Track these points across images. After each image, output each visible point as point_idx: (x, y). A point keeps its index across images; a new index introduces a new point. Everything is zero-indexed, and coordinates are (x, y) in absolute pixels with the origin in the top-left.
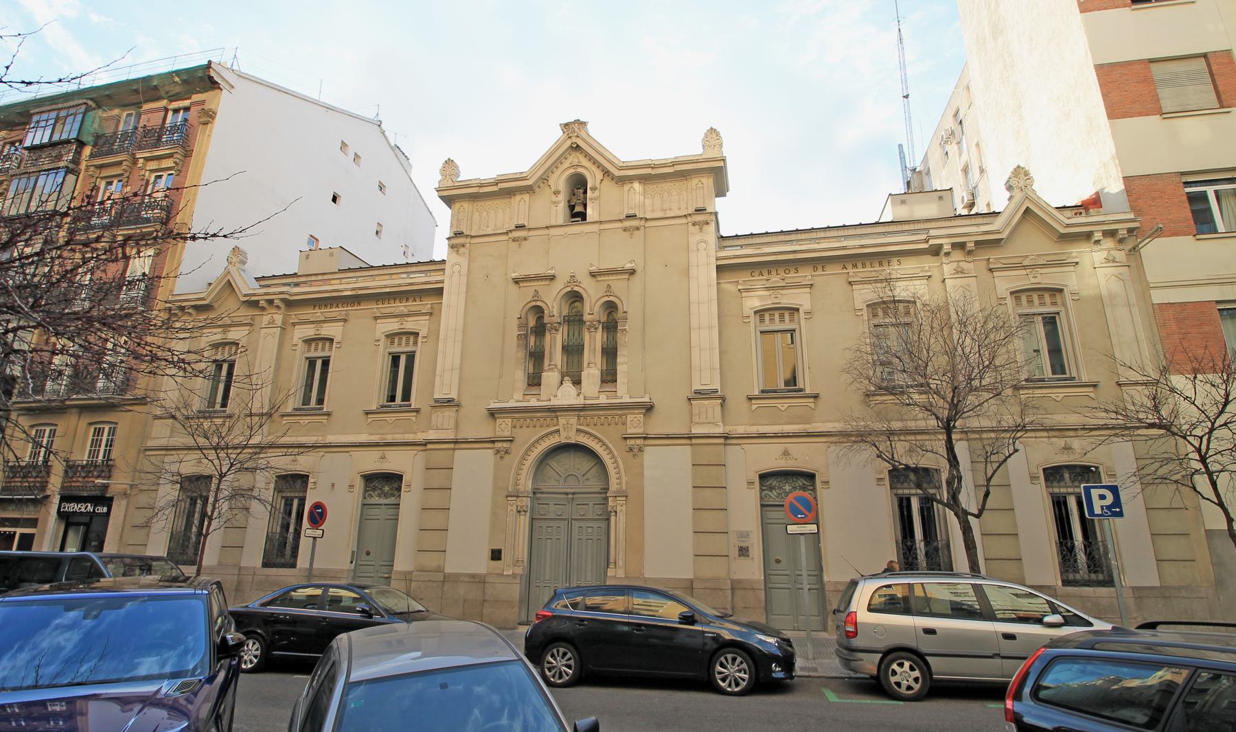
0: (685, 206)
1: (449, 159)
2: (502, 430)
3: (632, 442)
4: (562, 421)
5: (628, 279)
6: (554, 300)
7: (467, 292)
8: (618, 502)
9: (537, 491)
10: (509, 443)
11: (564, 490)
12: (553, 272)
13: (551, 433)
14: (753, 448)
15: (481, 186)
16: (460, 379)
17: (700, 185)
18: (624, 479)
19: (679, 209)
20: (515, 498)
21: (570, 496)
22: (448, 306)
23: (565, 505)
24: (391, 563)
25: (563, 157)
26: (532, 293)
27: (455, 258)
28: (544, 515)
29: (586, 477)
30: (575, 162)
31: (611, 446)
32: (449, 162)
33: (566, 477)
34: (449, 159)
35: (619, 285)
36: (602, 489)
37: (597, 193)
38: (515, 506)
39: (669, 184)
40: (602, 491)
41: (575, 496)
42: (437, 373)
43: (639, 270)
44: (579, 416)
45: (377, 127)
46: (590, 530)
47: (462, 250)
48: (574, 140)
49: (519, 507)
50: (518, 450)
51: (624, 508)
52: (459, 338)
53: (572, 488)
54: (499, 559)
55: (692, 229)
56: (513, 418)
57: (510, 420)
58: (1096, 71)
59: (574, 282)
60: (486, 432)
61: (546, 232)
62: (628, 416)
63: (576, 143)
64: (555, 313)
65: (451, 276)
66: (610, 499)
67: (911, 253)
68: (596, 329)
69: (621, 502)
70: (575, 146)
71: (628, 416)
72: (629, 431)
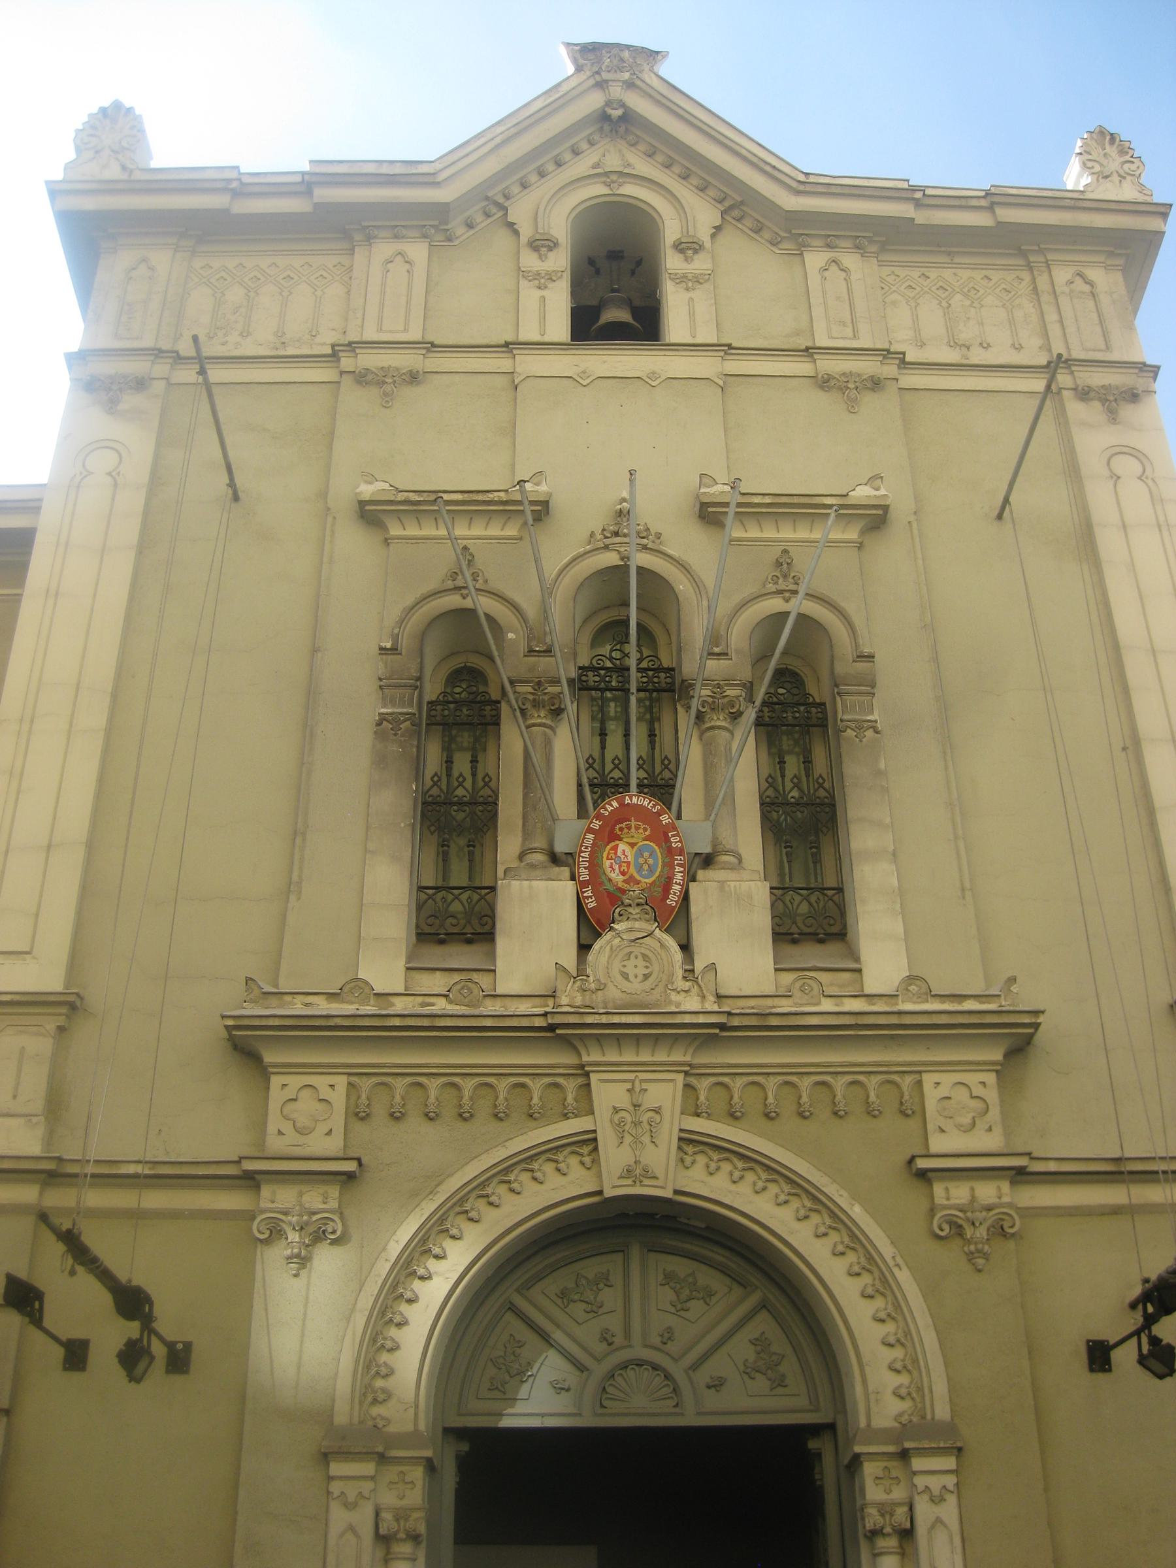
2: (300, 1131)
3: (959, 1193)
5: (860, 546)
10: (334, 1191)
12: (543, 488)
13: (552, 1150)
16: (86, 892)
17: (1080, 285)
19: (1018, 348)
20: (368, 1468)
26: (446, 557)
29: (703, 1376)
30: (613, 162)
37: (700, 264)
39: (965, 274)
43: (901, 508)
48: (616, 91)
49: (387, 1516)
51: (949, 1511)
52: (94, 716)
56: (355, 1073)
57: (341, 1081)
61: (502, 363)
62: (925, 1077)
63: (622, 105)
66: (870, 1469)
68: (736, 716)
69: (935, 1483)
70: (616, 113)
71: (928, 1080)
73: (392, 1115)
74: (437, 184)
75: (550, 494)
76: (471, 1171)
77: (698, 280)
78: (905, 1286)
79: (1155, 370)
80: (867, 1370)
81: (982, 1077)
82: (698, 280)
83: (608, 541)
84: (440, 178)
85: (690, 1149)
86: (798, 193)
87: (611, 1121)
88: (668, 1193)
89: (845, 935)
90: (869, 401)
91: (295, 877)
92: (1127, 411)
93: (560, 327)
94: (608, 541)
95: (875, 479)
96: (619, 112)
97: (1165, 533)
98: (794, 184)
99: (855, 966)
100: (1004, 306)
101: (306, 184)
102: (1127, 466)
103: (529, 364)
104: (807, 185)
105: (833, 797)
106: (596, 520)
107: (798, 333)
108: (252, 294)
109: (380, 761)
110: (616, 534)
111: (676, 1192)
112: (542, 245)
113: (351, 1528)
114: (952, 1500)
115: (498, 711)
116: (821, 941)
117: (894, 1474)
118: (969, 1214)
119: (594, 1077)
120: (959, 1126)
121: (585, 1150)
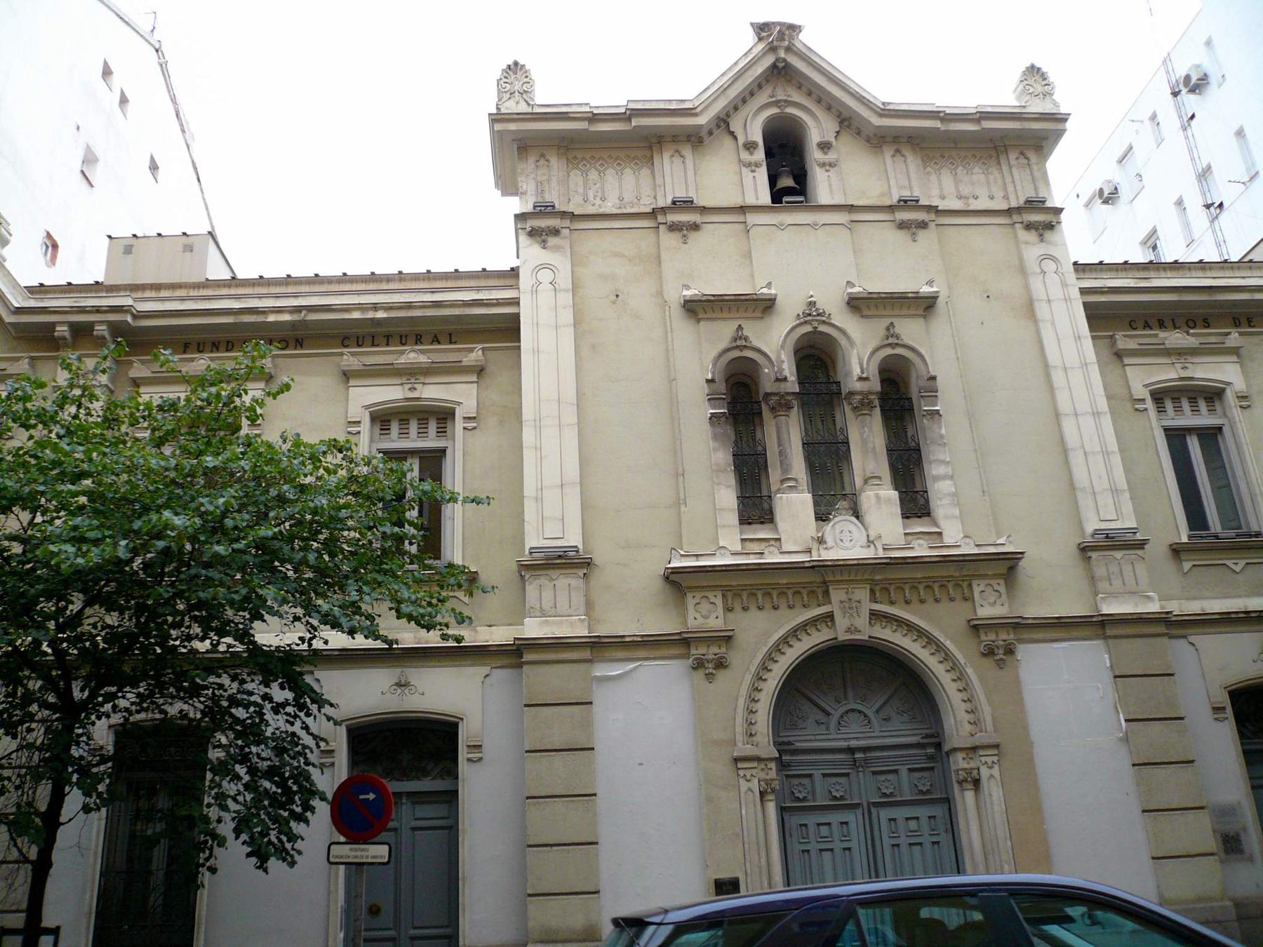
0: (1002, 194)
1: (710, 677)
4: (837, 595)
6: (782, 347)
7: (576, 324)
8: (983, 759)
9: (786, 747)
11: (844, 744)
13: (814, 622)
14: (1213, 644)
15: (594, 118)
16: (585, 507)
18: (987, 712)
19: (992, 198)
21: (858, 755)
22: (537, 352)
23: (847, 775)
24: (448, 931)
25: (759, 85)
27: (534, 253)
28: (805, 799)
30: (781, 96)
31: (948, 643)
32: (515, 68)
33: (853, 710)
34: (710, 677)
35: (910, 330)
36: (927, 736)
37: (831, 156)
38: (756, 781)
40: (925, 741)
41: (869, 755)
42: (526, 493)
44: (873, 583)
45: (154, 51)
47: (552, 241)
48: (782, 54)
50: (745, 660)
51: (996, 771)
52: (571, 417)
55: (1023, 235)
59: (818, 315)
60: (660, 623)
62: (973, 582)
63: (784, 60)
64: (787, 373)
65: (535, 291)
67: (485, 331)
69: (989, 760)
73: (743, 608)
74: (696, 115)
75: (776, 295)
76: (781, 632)
77: (832, 165)
78: (971, 676)
79: (1061, 210)
80: (956, 712)
81: (999, 581)
82: (832, 165)
83: (806, 319)
84: (698, 110)
85: (873, 617)
86: (881, 116)
87: (840, 607)
88: (867, 638)
89: (929, 513)
90: (922, 234)
91: (682, 496)
92: (1048, 235)
93: (765, 198)
94: (806, 319)
95: (930, 283)
96: (783, 64)
97: (1069, 303)
98: (878, 110)
99: (937, 530)
100: (983, 173)
101: (630, 114)
102: (1049, 266)
103: (752, 218)
104: (886, 112)
105: (919, 445)
106: (800, 308)
107: (882, 195)
108: (602, 175)
109: (715, 437)
110: (810, 315)
111: (870, 637)
112: (750, 146)
113: (750, 789)
114: (996, 767)
115: (760, 406)
116: (920, 517)
117: (970, 756)
118: (996, 643)
119: (831, 587)
120: (989, 603)
121: (828, 620)
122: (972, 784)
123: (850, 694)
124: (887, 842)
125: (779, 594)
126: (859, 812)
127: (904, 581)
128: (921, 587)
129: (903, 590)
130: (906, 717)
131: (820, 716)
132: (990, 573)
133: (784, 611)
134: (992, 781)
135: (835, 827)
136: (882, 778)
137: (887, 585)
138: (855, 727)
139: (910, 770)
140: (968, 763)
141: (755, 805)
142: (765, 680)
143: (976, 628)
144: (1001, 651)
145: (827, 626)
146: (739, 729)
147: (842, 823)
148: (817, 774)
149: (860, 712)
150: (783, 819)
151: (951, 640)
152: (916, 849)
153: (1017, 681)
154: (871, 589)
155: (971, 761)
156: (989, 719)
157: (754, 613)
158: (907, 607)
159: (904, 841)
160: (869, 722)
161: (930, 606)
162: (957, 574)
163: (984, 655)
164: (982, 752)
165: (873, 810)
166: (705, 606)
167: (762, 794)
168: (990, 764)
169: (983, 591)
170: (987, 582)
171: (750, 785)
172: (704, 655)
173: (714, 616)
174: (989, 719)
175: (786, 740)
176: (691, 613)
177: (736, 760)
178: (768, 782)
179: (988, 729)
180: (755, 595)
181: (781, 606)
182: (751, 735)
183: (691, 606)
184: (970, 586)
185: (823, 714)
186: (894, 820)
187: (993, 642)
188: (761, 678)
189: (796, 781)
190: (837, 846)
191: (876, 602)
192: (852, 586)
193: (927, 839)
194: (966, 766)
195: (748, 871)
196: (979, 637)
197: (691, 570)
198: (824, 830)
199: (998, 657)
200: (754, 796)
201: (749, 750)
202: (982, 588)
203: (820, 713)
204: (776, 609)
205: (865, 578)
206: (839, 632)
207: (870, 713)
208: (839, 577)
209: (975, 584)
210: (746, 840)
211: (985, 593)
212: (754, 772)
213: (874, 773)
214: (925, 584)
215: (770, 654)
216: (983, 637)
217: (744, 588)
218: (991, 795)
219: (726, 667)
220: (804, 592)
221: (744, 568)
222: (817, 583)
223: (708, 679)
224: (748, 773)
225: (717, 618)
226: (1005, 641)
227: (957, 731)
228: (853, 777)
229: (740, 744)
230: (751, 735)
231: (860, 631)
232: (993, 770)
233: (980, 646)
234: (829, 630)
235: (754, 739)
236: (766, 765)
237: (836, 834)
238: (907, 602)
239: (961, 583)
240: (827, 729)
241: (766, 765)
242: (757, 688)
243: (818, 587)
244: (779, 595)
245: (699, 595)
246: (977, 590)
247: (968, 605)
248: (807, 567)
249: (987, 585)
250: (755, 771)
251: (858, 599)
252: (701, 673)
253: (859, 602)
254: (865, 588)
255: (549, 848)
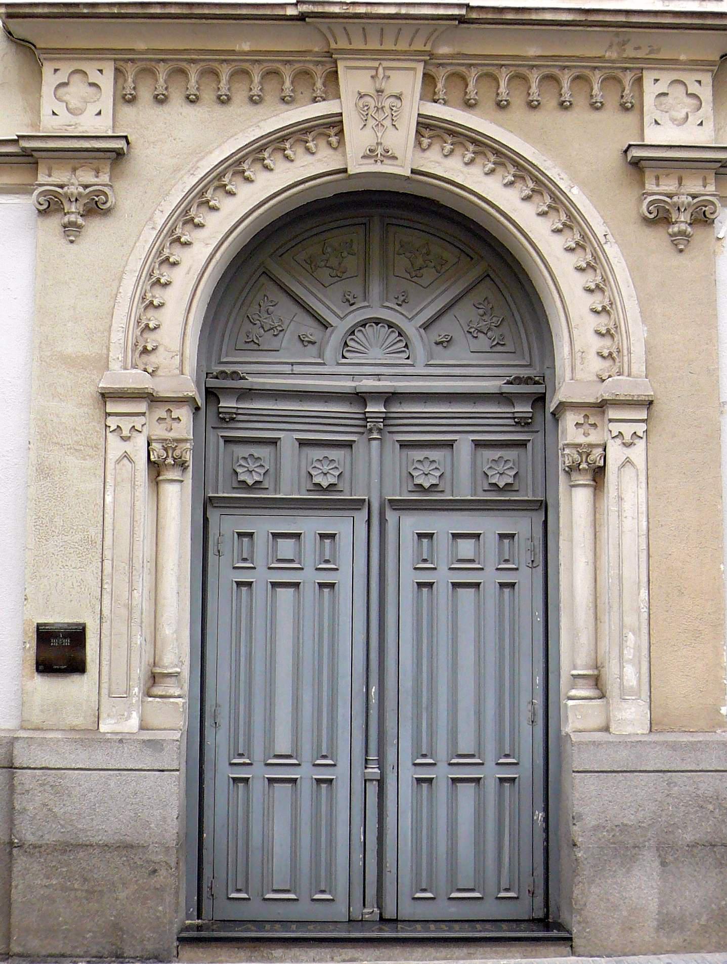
1: (71, 230)
8: (615, 428)
11: (346, 385)
21: (373, 408)
23: (349, 445)
31: (575, 194)
33: (377, 322)
34: (71, 230)
36: (518, 380)
38: (140, 441)
41: (396, 408)
44: (430, 59)
46: (466, 548)
53: (378, 376)
54: (77, 666)
58: (32, 645)
69: (627, 430)
72: (653, 136)
85: (427, 133)
88: (408, 173)
111: (413, 171)
113: (126, 456)
117: (591, 421)
119: (341, 66)
120: (673, 120)
121: (332, 131)
122: (589, 477)
123: (375, 289)
124: (409, 578)
125: (232, 75)
126: (362, 515)
127: (500, 62)
128: (534, 78)
129: (496, 80)
130: (483, 342)
131: (311, 330)
132: (683, 57)
133: (239, 108)
134: (629, 471)
135: (309, 542)
136: (419, 454)
137: (463, 69)
138: (376, 354)
139: (478, 444)
140: (586, 434)
141: (133, 487)
142: (187, 244)
143: (637, 165)
144: (684, 217)
145: (330, 144)
146: (117, 337)
147: (323, 536)
148: (288, 440)
149: (391, 325)
150: (206, 520)
151: (583, 185)
152: (467, 594)
153: (710, 281)
154: (425, 75)
155: (592, 431)
156: (638, 351)
157: (177, 107)
158: (500, 115)
159: (443, 578)
160: (406, 346)
161: (548, 117)
162: (612, 54)
163: (650, 222)
164: (612, 414)
165: (391, 516)
166: (77, 91)
167: (155, 468)
168: (628, 438)
169: (665, 94)
170: (675, 76)
171: (127, 447)
172: (62, 187)
173: (92, 109)
174: (638, 351)
175: (229, 369)
176: (48, 103)
177: (106, 396)
178: (169, 445)
179: (635, 369)
180: (183, 72)
181: (608, 105)
182: (145, 351)
183: (47, 89)
184: (639, 81)
185: (315, 324)
186: (430, 536)
187: (670, 196)
188: (178, 239)
189: (242, 451)
190: (309, 577)
191: (435, 101)
192: (386, 64)
193: (490, 578)
194: (581, 440)
195: (106, 612)
196: (643, 185)
197: (46, 10)
198: (286, 548)
199: (675, 229)
200: (134, 470)
201: (135, 379)
202: (662, 87)
203: (310, 321)
204: (223, 102)
205: (413, 48)
206: (349, 161)
207: (410, 329)
208: (358, 44)
209: (648, 78)
210: (108, 554)
211: (669, 100)
212: (138, 422)
213: (404, 445)
214: (576, 72)
215: (202, 193)
216: (650, 186)
217: (162, 56)
218: (620, 499)
219: (107, 213)
220: (287, 73)
221: (158, 10)
222: (317, 54)
223: (66, 234)
224: (126, 424)
225: (99, 113)
226: (694, 197)
227: (573, 369)
228: (360, 449)
229: (115, 366)
230: (145, 351)
231: (395, 158)
232: (633, 448)
233: (641, 201)
234: (331, 152)
235: (153, 359)
236: (169, 411)
237: (309, 559)
238: (501, 106)
239: (620, 74)
240: (320, 355)
241: (169, 411)
242: (167, 259)
243: (317, 63)
244: (203, 73)
245: (66, 68)
246: (650, 90)
247: (630, 119)
248: (292, 18)
249: (674, 82)
250: (142, 420)
251: (396, 91)
252: (54, 223)
253: (398, 97)
254: (414, 69)
255: (652, 703)
